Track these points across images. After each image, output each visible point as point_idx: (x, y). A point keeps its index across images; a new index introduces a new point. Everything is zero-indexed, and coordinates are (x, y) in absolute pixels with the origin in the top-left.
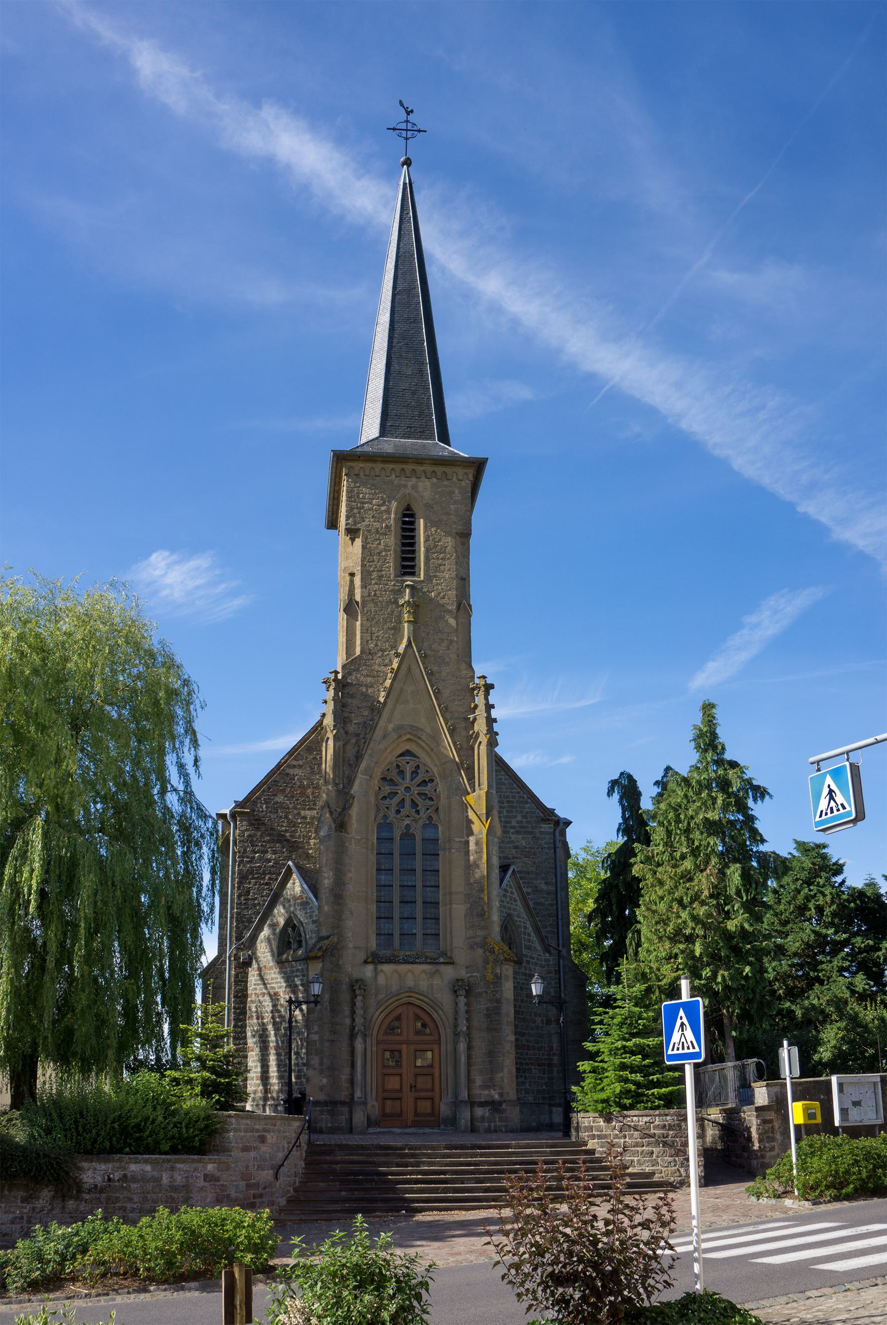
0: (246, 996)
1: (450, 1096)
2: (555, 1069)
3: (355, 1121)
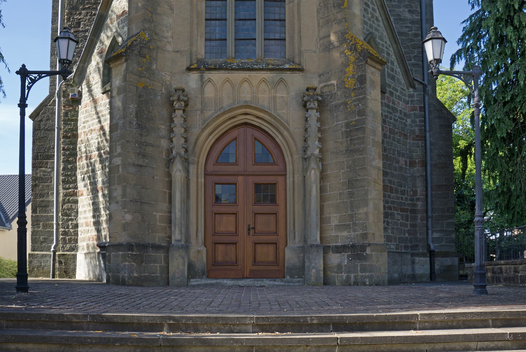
0: (76, 136)
1: (297, 240)
2: (419, 216)
3: (172, 269)
